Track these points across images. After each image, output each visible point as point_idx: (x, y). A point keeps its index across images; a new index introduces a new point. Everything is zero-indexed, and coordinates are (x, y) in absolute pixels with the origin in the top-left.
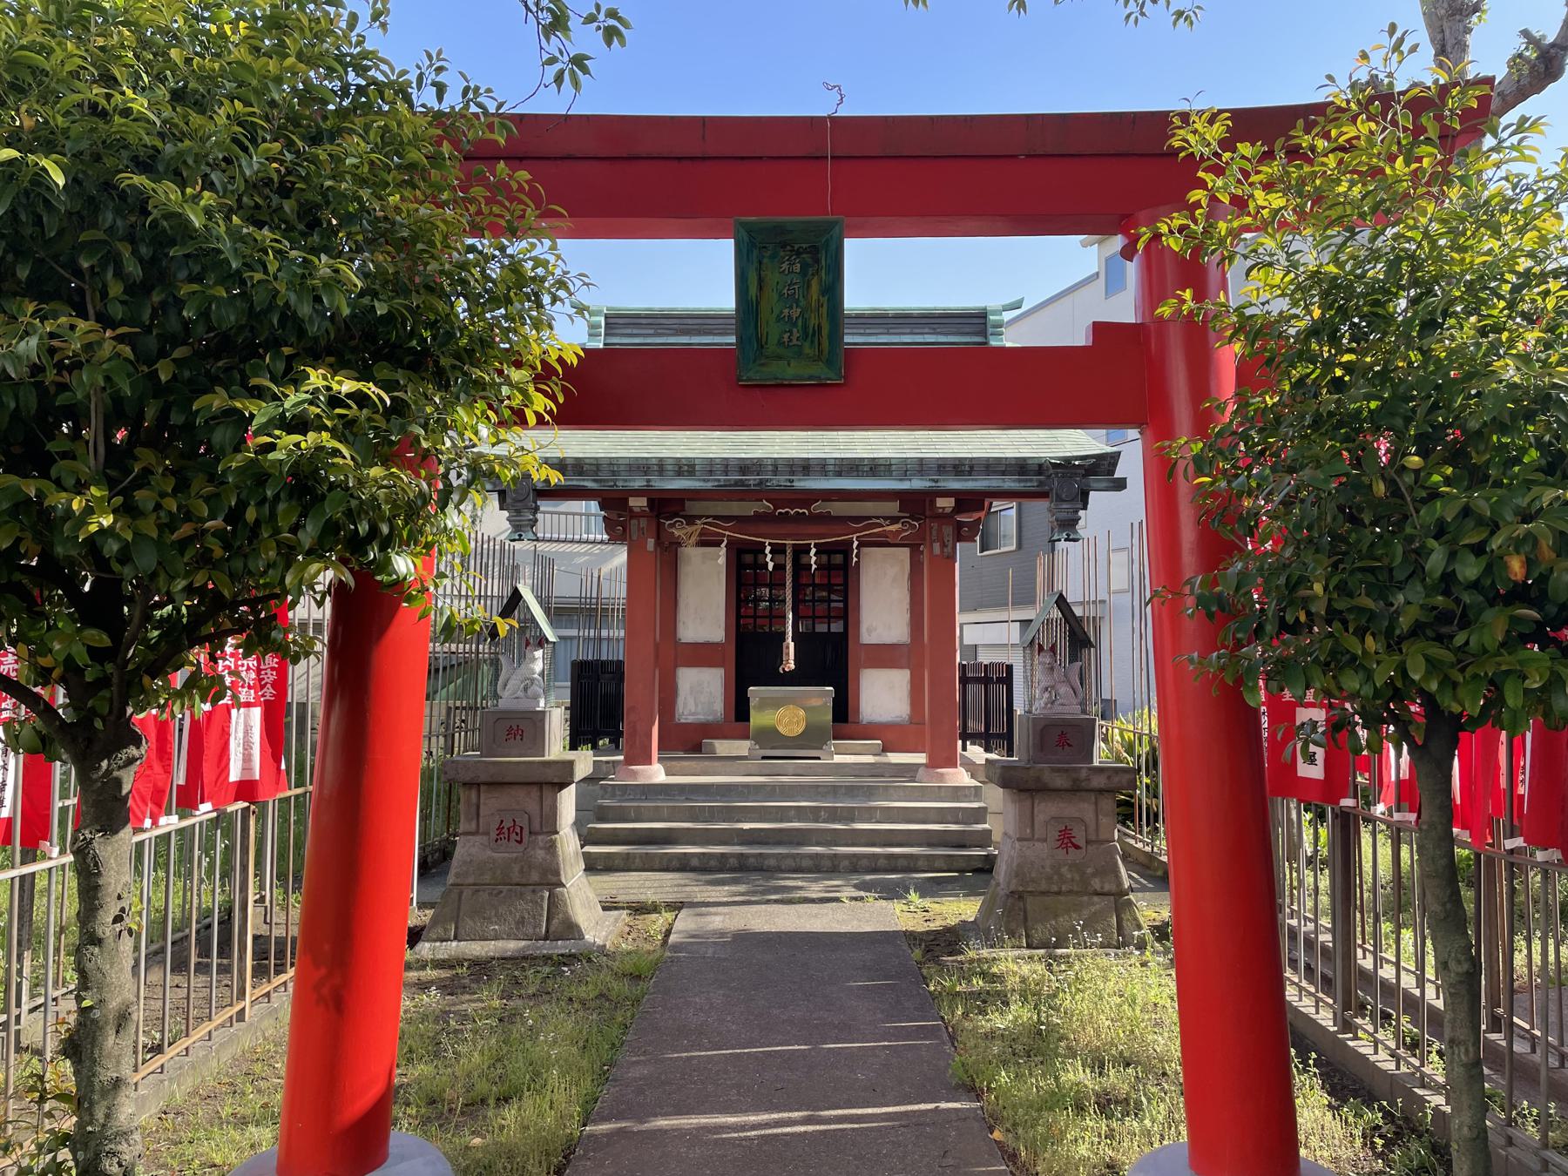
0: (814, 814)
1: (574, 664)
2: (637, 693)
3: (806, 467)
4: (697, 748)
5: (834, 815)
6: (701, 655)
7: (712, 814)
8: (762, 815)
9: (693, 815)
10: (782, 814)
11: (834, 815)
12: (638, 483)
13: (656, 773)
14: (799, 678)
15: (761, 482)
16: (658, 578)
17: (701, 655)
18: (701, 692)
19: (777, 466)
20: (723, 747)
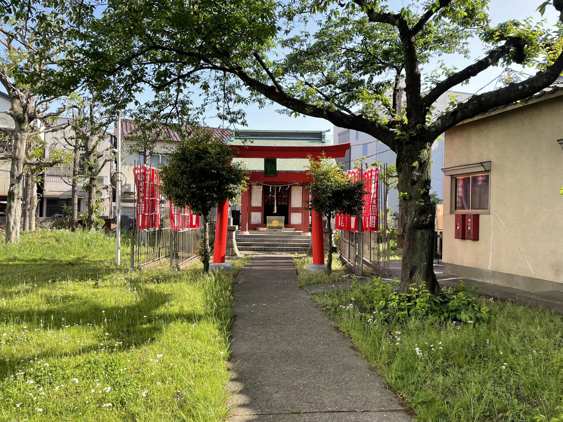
0: (280, 241)
4: (255, 229)
5: (283, 241)
6: (256, 209)
10: (273, 241)
13: (247, 233)
17: (256, 209)
20: (261, 229)
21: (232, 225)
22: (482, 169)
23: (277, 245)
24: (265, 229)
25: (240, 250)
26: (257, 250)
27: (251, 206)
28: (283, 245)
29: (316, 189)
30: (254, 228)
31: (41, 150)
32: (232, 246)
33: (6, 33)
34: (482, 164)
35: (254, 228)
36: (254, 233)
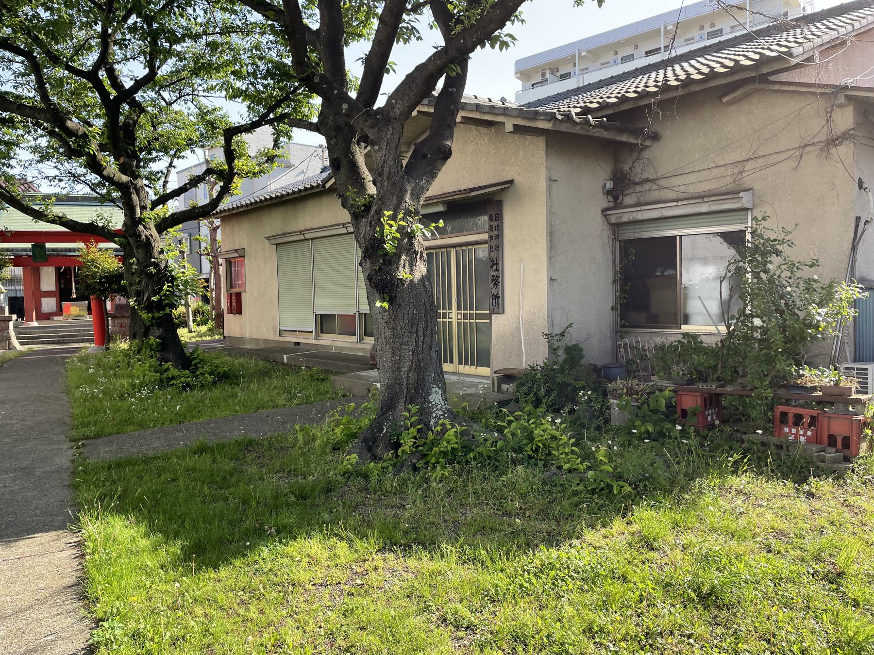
0: (79, 331)
1: (503, 313)
2: (28, 304)
3: (70, 250)
4: (48, 319)
5: (84, 331)
6: (48, 294)
7: (51, 332)
8: (64, 331)
9: (46, 332)
10: (70, 331)
11: (84, 331)
12: (24, 254)
13: (35, 324)
14: (491, 320)
15: (235, 150)
16: (35, 276)
17: (48, 294)
18: (49, 304)
19: (62, 249)
20: (55, 318)
21: (7, 314)
22: (236, 255)
23: (75, 336)
24: (60, 318)
25: (22, 344)
26: (48, 343)
27: (41, 291)
28: (84, 335)
29: (623, 326)
30: (42, 317)
31: (100, 609)
32: (9, 338)
33: (41, 602)
34: (236, 251)
35: (48, 317)
36: (45, 324)
